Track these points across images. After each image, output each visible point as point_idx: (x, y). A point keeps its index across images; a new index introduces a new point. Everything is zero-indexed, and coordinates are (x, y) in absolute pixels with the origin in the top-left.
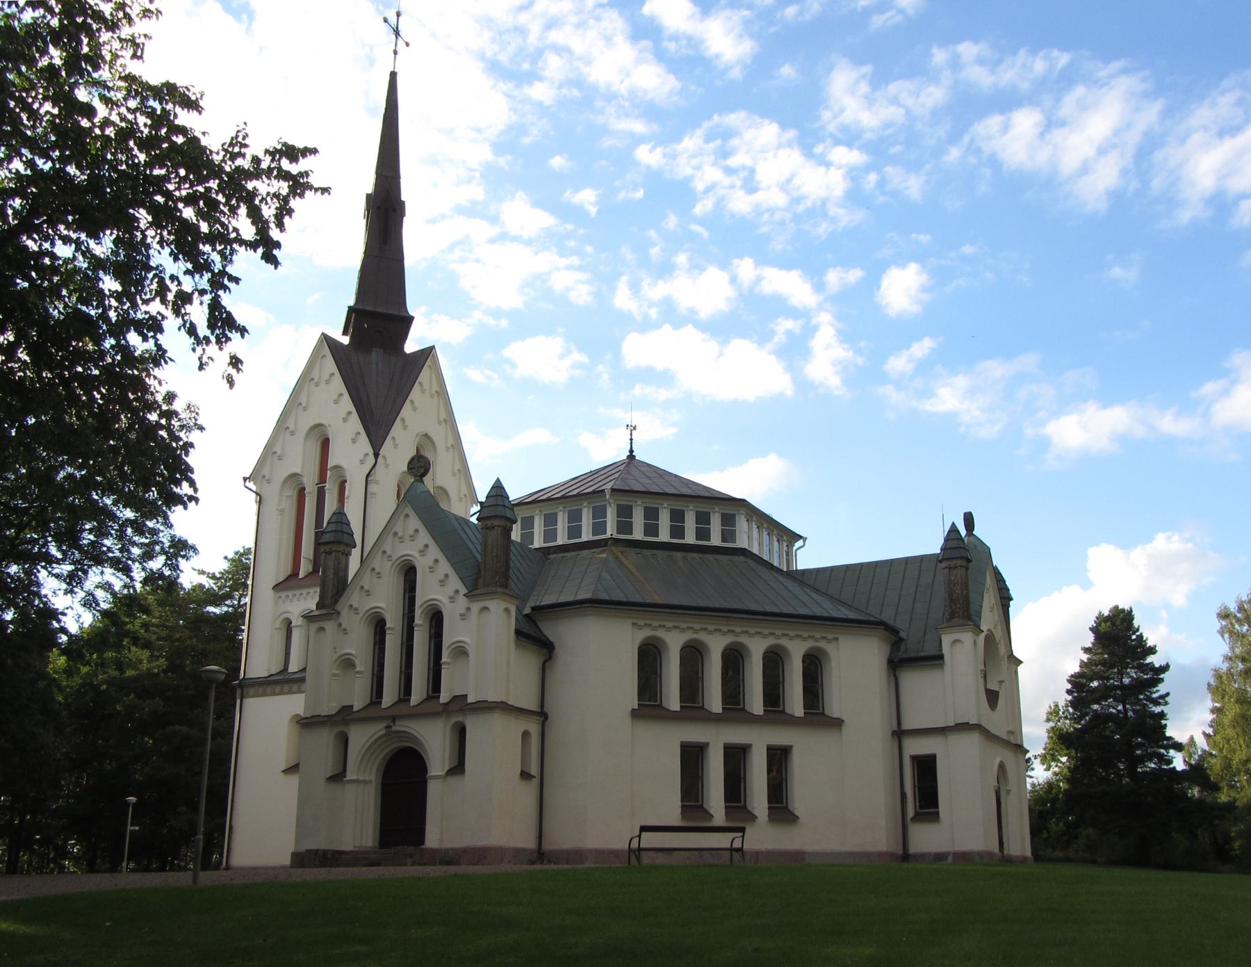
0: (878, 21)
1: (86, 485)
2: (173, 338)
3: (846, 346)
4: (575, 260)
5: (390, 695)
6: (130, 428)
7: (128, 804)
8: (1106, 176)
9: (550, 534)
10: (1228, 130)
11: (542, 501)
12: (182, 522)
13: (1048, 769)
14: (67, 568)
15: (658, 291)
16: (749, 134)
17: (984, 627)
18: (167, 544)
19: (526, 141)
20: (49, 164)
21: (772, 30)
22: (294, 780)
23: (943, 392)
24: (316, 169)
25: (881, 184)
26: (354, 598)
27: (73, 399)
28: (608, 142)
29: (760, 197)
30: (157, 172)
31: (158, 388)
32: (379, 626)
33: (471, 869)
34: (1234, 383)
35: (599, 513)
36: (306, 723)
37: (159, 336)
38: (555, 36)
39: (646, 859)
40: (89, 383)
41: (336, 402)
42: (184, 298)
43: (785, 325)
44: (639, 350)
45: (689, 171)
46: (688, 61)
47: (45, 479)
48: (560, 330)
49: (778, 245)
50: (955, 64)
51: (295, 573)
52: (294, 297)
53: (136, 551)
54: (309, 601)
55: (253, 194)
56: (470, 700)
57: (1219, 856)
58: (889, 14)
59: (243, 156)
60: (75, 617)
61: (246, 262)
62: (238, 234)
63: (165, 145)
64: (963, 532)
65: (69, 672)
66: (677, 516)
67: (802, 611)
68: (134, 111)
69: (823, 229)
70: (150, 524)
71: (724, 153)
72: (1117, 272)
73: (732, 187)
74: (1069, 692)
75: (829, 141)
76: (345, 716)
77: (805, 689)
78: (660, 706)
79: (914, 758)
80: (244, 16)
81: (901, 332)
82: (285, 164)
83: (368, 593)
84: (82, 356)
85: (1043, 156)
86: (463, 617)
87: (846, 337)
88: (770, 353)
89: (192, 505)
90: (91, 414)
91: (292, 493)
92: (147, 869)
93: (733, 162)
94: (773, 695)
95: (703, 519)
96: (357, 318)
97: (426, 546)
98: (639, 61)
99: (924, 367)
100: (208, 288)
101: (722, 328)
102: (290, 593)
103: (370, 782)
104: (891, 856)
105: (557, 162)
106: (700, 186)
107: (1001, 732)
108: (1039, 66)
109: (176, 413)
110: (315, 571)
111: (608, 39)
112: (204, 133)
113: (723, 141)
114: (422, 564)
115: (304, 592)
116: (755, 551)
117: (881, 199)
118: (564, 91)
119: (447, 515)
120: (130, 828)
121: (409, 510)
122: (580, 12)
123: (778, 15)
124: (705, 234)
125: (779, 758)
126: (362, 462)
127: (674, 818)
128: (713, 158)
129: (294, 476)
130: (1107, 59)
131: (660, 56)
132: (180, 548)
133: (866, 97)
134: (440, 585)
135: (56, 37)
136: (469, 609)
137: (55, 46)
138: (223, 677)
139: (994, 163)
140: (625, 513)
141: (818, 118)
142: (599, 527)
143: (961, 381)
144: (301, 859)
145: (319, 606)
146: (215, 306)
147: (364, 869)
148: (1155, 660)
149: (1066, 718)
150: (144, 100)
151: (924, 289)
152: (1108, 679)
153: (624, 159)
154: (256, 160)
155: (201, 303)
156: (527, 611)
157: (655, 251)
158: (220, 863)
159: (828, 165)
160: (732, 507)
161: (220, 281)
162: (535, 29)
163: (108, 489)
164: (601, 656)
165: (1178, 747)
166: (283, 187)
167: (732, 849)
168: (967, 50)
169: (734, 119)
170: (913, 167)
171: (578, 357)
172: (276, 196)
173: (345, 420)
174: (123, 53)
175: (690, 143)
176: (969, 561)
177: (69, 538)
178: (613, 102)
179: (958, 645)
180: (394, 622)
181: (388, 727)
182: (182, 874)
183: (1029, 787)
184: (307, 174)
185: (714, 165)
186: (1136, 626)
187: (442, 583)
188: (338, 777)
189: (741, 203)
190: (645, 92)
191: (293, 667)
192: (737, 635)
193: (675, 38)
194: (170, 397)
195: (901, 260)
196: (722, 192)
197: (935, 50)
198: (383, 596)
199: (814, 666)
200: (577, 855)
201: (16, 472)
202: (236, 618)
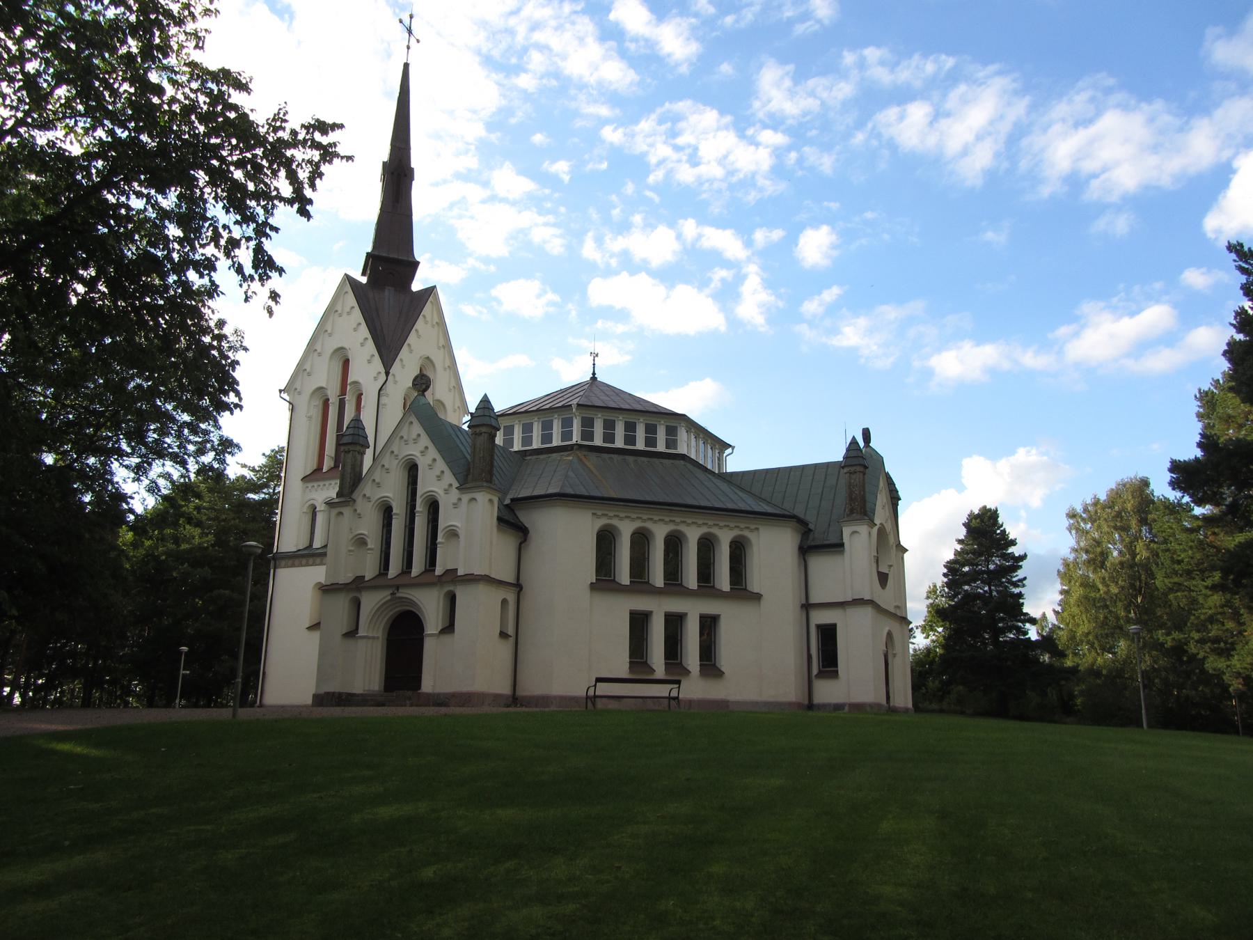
0: (800, 29)
2: (224, 275)
4: (551, 218)
5: (394, 569)
6: (188, 348)
7: (181, 653)
8: (983, 158)
9: (527, 440)
10: (1082, 122)
11: (520, 413)
12: (229, 425)
13: (927, 637)
14: (135, 460)
15: (618, 244)
16: (694, 119)
17: (877, 521)
18: (216, 443)
19: (513, 121)
20: (127, 133)
21: (714, 34)
22: (316, 635)
24: (340, 140)
25: (800, 161)
26: (367, 489)
28: (579, 123)
29: (702, 169)
30: (213, 141)
32: (387, 511)
33: (458, 710)
34: (1083, 327)
35: (567, 423)
36: (327, 590)
38: (538, 37)
39: (600, 704)
40: (155, 311)
41: (355, 330)
42: (234, 243)
43: (721, 274)
44: (601, 292)
45: (645, 148)
46: (645, 59)
48: (538, 274)
49: (716, 209)
50: (862, 65)
52: (324, 243)
53: (191, 448)
54: (331, 490)
55: (291, 160)
56: (460, 573)
57: (1065, 710)
58: (809, 23)
59: (284, 129)
60: (141, 501)
61: (284, 215)
64: (862, 444)
65: (135, 545)
66: (631, 427)
67: (730, 506)
68: (195, 91)
69: (752, 196)
70: (203, 426)
71: (673, 134)
72: (990, 235)
73: (679, 161)
74: (945, 575)
76: (358, 585)
79: (819, 627)
80: (286, 16)
81: (814, 281)
82: (318, 136)
85: (931, 141)
86: (455, 505)
87: (769, 284)
88: (708, 296)
89: (237, 411)
90: (157, 336)
91: (318, 403)
92: (196, 706)
93: (680, 141)
94: (706, 573)
95: (651, 430)
96: (373, 262)
98: (606, 58)
99: (832, 310)
100: (253, 235)
101: (669, 276)
102: (316, 484)
104: (799, 705)
105: (538, 138)
106: (653, 160)
107: (887, 604)
108: (930, 68)
109: (225, 337)
110: (336, 466)
111: (581, 40)
114: (422, 463)
115: (327, 483)
116: (693, 456)
117: (800, 173)
118: (544, 81)
120: (182, 672)
121: (413, 419)
122: (559, 17)
123: (719, 23)
124: (657, 199)
125: (709, 625)
126: (376, 379)
127: (624, 672)
128: (664, 137)
131: (623, 54)
132: (227, 446)
134: (437, 479)
135: (134, 30)
136: (460, 499)
138: (260, 551)
139: (892, 146)
140: (588, 424)
141: (750, 106)
142: (567, 435)
143: (862, 322)
144: (321, 700)
145: (338, 495)
146: (259, 250)
148: (1015, 550)
150: (204, 82)
151: (833, 247)
152: (977, 565)
153: (592, 137)
154: (294, 133)
156: (507, 501)
157: (616, 212)
159: (757, 144)
160: (675, 421)
161: (263, 230)
162: (522, 31)
163: (170, 397)
164: (566, 538)
165: (1033, 621)
166: (316, 155)
167: (670, 698)
168: (872, 53)
169: (682, 106)
170: (827, 147)
172: (310, 162)
173: (362, 344)
175: (645, 125)
176: (866, 467)
177: (137, 436)
180: (399, 509)
181: (393, 594)
182: (223, 710)
184: (335, 145)
187: (439, 478)
188: (351, 634)
189: (686, 175)
193: (635, 40)
195: (815, 223)
196: (671, 165)
197: (845, 53)
198: (392, 488)
199: (739, 551)
200: (544, 700)
201: (95, 382)
202: (271, 504)
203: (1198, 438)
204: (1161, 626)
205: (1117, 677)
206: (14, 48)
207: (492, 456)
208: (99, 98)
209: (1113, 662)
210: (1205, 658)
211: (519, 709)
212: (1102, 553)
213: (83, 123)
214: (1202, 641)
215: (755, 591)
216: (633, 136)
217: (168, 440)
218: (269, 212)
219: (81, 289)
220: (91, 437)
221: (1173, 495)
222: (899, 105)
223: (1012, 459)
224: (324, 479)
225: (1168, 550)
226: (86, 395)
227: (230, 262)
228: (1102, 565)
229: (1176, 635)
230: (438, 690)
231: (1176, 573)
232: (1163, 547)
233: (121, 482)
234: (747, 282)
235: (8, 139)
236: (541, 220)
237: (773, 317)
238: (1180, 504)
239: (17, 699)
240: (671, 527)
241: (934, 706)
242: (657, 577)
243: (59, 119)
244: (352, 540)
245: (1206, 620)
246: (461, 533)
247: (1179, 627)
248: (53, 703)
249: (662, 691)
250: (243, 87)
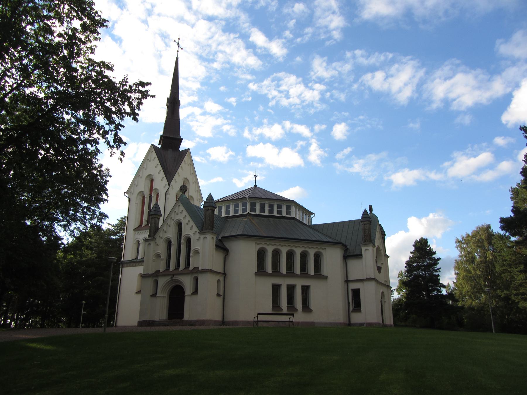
0: (328, 43)
2: (102, 146)
4: (229, 121)
5: (172, 267)
7: (82, 304)
9: (228, 212)
12: (103, 207)
13: (399, 294)
14: (64, 223)
15: (258, 131)
16: (286, 80)
17: (376, 245)
18: (98, 215)
19: (212, 81)
20: (62, 88)
21: (293, 46)
22: (139, 296)
23: (356, 166)
25: (332, 96)
26: (161, 234)
27: (68, 166)
28: (239, 82)
30: (98, 91)
33: (199, 328)
34: (454, 162)
35: (244, 205)
36: (144, 276)
38: (221, 48)
39: (260, 324)
40: (74, 161)
41: (156, 167)
43: (300, 143)
44: (252, 151)
45: (266, 92)
46: (265, 56)
47: (58, 192)
49: (298, 116)
50: (354, 57)
51: (141, 225)
53: (88, 217)
54: (145, 234)
56: (200, 269)
57: (459, 325)
58: (331, 41)
59: (126, 85)
60: (67, 239)
61: (128, 120)
64: (369, 212)
65: (64, 258)
66: (271, 206)
67: (314, 239)
69: (312, 111)
70: (93, 208)
71: (278, 86)
72: (411, 125)
73: (281, 97)
74: (406, 267)
76: (157, 274)
77: (315, 266)
79: (352, 290)
81: (340, 145)
82: (140, 88)
83: (166, 232)
84: (71, 152)
85: (386, 86)
86: (198, 240)
87: (321, 147)
88: (296, 152)
89: (106, 202)
91: (140, 197)
92: (89, 327)
93: (282, 88)
94: (304, 267)
95: (280, 207)
96: (163, 139)
98: (248, 56)
101: (279, 144)
102: (139, 232)
104: (345, 324)
105: (222, 88)
106: (270, 97)
107: (382, 280)
108: (382, 58)
109: (102, 171)
110: (148, 224)
111: (238, 49)
114: (184, 222)
115: (144, 231)
116: (298, 218)
117: (332, 101)
118: (224, 65)
119: (193, 206)
120: (83, 312)
121: (180, 204)
122: (228, 40)
123: (295, 41)
125: (306, 289)
126: (164, 187)
127: (270, 311)
128: (274, 87)
129: (141, 192)
130: (405, 55)
131: (255, 54)
132: (102, 216)
133: (325, 67)
134: (190, 229)
135: (66, 46)
137: (66, 49)
139: (370, 89)
140: (253, 205)
141: (309, 74)
142: (244, 210)
143: (361, 161)
144: (141, 324)
145: (149, 236)
146: (116, 135)
148: (435, 256)
151: (348, 131)
152: (419, 263)
153: (244, 88)
154: (131, 87)
156: (220, 238)
157: (256, 118)
159: (313, 90)
160: (290, 203)
161: (118, 127)
162: (214, 46)
163: (79, 196)
164: (245, 254)
165: (444, 287)
166: (140, 96)
167: (289, 321)
168: (358, 52)
169: (281, 74)
170: (342, 90)
171: (231, 153)
172: (137, 98)
175: (266, 82)
176: (371, 222)
177: (65, 213)
179: (367, 251)
180: (174, 242)
181: (171, 278)
183: (392, 300)
184: (147, 91)
185: (275, 90)
187: (191, 229)
188: (154, 295)
189: (285, 102)
190: (251, 66)
191: (140, 257)
192: (292, 247)
193: (260, 48)
194: (101, 166)
196: (278, 99)
197: (347, 53)
198: (171, 233)
199: (318, 258)
200: (236, 323)
201: (48, 190)
202: (120, 240)
203: (511, 208)
204: (500, 288)
205: (481, 309)
206: (17, 55)
207: (213, 220)
208: (52, 74)
209: (479, 304)
210: (518, 302)
211: (225, 327)
212: (472, 257)
213: (45, 85)
214: (517, 295)
216: (261, 87)
217: (78, 214)
219: (43, 152)
221: (502, 232)
223: (428, 218)
224: (142, 230)
225: (501, 255)
226: (45, 196)
227: (104, 140)
228: (473, 262)
229: (505, 292)
231: (504, 265)
232: (499, 254)
233: (58, 232)
234: (312, 146)
236: (225, 122)
237: (324, 160)
238: (505, 236)
239: (13, 325)
240: (289, 248)
241: (403, 324)
242: (283, 269)
243: (35, 83)
244: (155, 256)
245: (519, 285)
246: (200, 251)
247: (507, 288)
248: (28, 326)
250: (110, 69)
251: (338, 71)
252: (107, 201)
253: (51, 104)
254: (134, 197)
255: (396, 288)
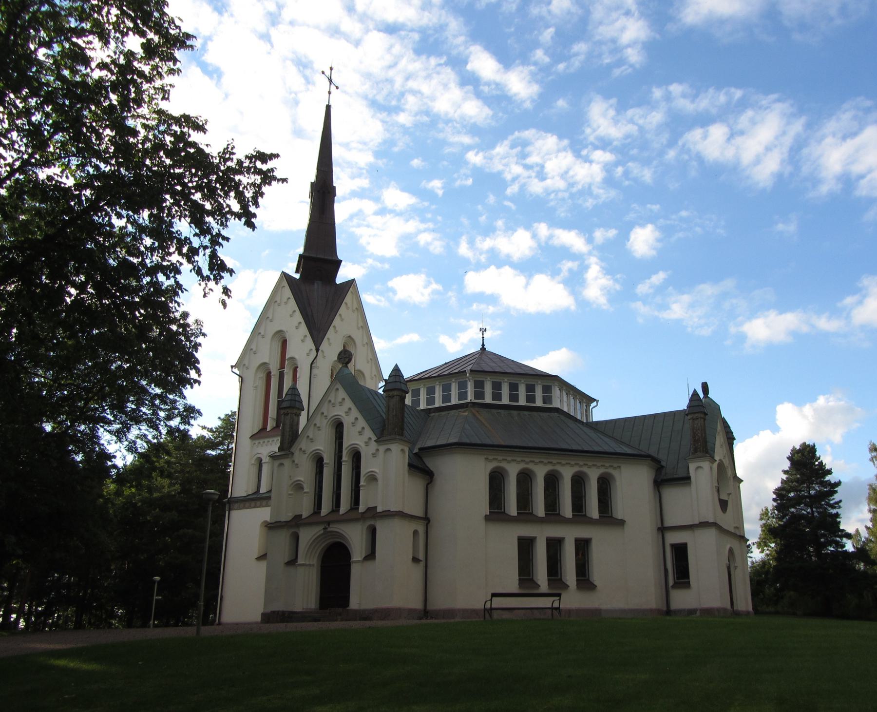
0: (617, 72)
1: (130, 373)
2: (187, 277)
3: (609, 277)
4: (431, 225)
6: (161, 334)
7: (154, 582)
8: (772, 165)
9: (430, 401)
10: (846, 136)
11: (426, 379)
12: (192, 396)
13: (762, 552)
14: (116, 426)
15: (487, 244)
16: (539, 143)
17: (717, 458)
18: (182, 410)
19: (396, 149)
20: (108, 168)
21: (550, 78)
22: (263, 565)
23: (676, 307)
24: (278, 166)
25: (626, 174)
26: (302, 444)
27: (123, 317)
28: (448, 150)
29: (549, 182)
30: (177, 171)
31: (178, 308)
32: (319, 462)
33: (380, 623)
34: (865, 296)
35: (462, 386)
36: (271, 527)
37: (177, 276)
38: (411, 84)
39: (496, 615)
41: (291, 316)
42: (194, 252)
43: (568, 265)
44: (475, 282)
45: (500, 167)
46: (497, 98)
47: (103, 368)
48: (423, 270)
49: (562, 213)
50: (668, 98)
51: (264, 428)
52: (265, 247)
53: (162, 414)
54: (273, 446)
55: (239, 183)
56: (379, 510)
58: (624, 68)
59: (232, 160)
60: (122, 457)
61: (235, 228)
62: (230, 209)
63: (183, 154)
64: (701, 395)
65: (118, 493)
66: (514, 387)
67: (597, 449)
68: (163, 133)
69: (589, 203)
70: (171, 397)
71: (524, 156)
72: (780, 227)
73: (529, 177)
74: (774, 500)
75: (590, 147)
76: (297, 522)
78: (504, 512)
79: (672, 546)
80: (215, 76)
81: (645, 268)
82: (259, 164)
83: (312, 440)
85: (730, 153)
86: (374, 455)
87: (608, 271)
88: (559, 283)
89: (196, 385)
90: (135, 326)
91: (262, 375)
92: (167, 625)
94: (579, 504)
95: (530, 389)
96: (304, 262)
97: (350, 409)
98: (464, 99)
99: (660, 290)
100: (209, 245)
101: (527, 267)
103: (313, 565)
104: (659, 611)
105: (416, 162)
106: (508, 177)
107: (729, 525)
108: (722, 98)
109: (188, 325)
110: (278, 426)
111: (445, 86)
112: (207, 145)
113: (522, 149)
114: (347, 421)
116: (565, 409)
117: (627, 183)
118: (418, 118)
119: (363, 388)
120: (155, 597)
121: (339, 386)
122: (427, 69)
123: (554, 69)
124: (513, 206)
125: (583, 546)
126: (308, 355)
127: (514, 587)
128: (515, 159)
131: (478, 95)
132: (190, 412)
133: (613, 119)
134: (359, 435)
135: (115, 87)
136: (378, 450)
137: (114, 93)
138: (217, 497)
139: (699, 158)
140: (479, 385)
141: (583, 132)
143: (686, 298)
144: (268, 617)
145: (280, 449)
146: (214, 256)
147: (310, 623)
149: (773, 517)
150: (169, 125)
151: (658, 240)
152: (800, 491)
153: (459, 160)
154: (240, 163)
155: (204, 255)
156: (416, 451)
157: (483, 219)
158: (214, 620)
159: (591, 162)
160: (550, 381)
161: (216, 240)
162: (399, 82)
163: (145, 375)
164: (465, 481)
165: (849, 536)
166: (258, 179)
167: (552, 608)
168: (676, 89)
169: (529, 134)
170: (646, 162)
171: (435, 286)
172: (253, 185)
173: (297, 328)
174: (157, 96)
175: (500, 149)
176: (706, 414)
177: (119, 407)
178: (450, 125)
179: (700, 471)
181: (325, 529)
182: (189, 629)
183: (749, 564)
184: (272, 170)
185: (517, 163)
186: (818, 455)
187: (361, 433)
188: (292, 562)
189: (536, 187)
190: (471, 118)
191: (263, 489)
192: (554, 465)
193: (488, 84)
194: (185, 315)
195: (642, 222)
196: (523, 181)
197: (654, 90)
198: (323, 443)
199: (605, 485)
200: (450, 613)
201: (85, 364)
202: (226, 458)
206: (21, 106)
211: (429, 621)
213: (74, 162)
215: (620, 518)
216: (491, 159)
217: (144, 409)
218: (224, 225)
219: (73, 291)
220: (81, 408)
222: (702, 127)
223: (815, 405)
227: (191, 266)
230: (363, 607)
233: (106, 444)
235: (17, 175)
236: (422, 226)
237: (613, 298)
239: (22, 624)
241: (772, 609)
243: (57, 159)
246: (379, 477)
248: (51, 626)
249: (545, 602)
250: (200, 128)
251: (637, 124)
252: (199, 383)
253: (87, 199)
254: (250, 375)
255: (756, 540)
